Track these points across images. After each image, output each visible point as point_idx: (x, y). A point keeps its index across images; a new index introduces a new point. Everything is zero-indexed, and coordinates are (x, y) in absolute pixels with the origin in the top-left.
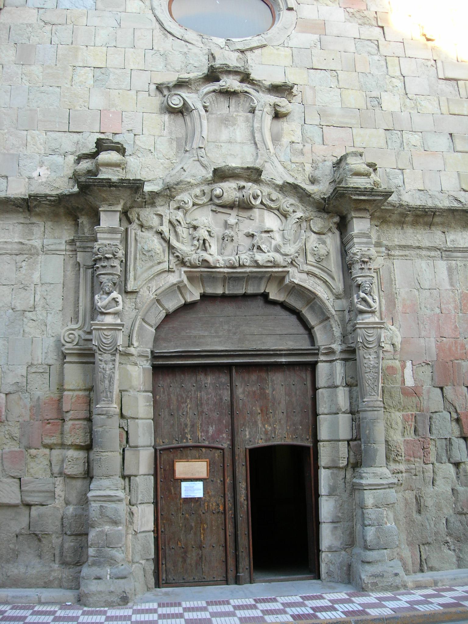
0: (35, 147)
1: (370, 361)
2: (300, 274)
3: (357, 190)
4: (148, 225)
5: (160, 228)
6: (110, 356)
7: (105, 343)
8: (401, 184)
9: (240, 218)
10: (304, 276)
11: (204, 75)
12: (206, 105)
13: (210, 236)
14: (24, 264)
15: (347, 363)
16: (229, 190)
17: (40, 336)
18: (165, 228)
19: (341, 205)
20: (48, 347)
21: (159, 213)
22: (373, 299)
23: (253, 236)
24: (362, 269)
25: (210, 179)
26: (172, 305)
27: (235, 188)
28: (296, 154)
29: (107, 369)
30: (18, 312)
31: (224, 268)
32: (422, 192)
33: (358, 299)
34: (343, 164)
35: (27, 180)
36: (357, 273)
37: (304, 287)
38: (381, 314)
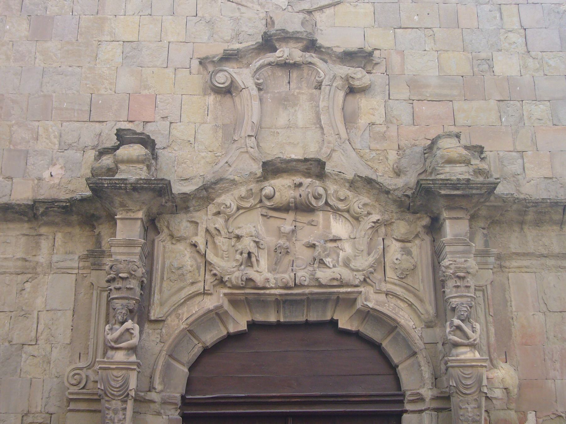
0: (47, 141)
1: (468, 412)
2: (377, 295)
3: (446, 183)
4: (179, 235)
5: (195, 239)
7: (113, 387)
8: (520, 171)
9: (298, 224)
10: (382, 297)
11: (257, 45)
12: (259, 82)
13: (259, 247)
15: (441, 414)
16: (282, 188)
19: (425, 202)
20: (51, 390)
21: (193, 219)
22: (473, 327)
23: (313, 246)
24: (457, 287)
25: (259, 174)
26: (211, 337)
27: (290, 186)
28: (376, 138)
30: (16, 346)
31: (276, 288)
32: (550, 181)
33: (451, 327)
34: (400, 147)
35: (36, 182)
36: (451, 292)
37: (381, 312)
38: (489, 347)
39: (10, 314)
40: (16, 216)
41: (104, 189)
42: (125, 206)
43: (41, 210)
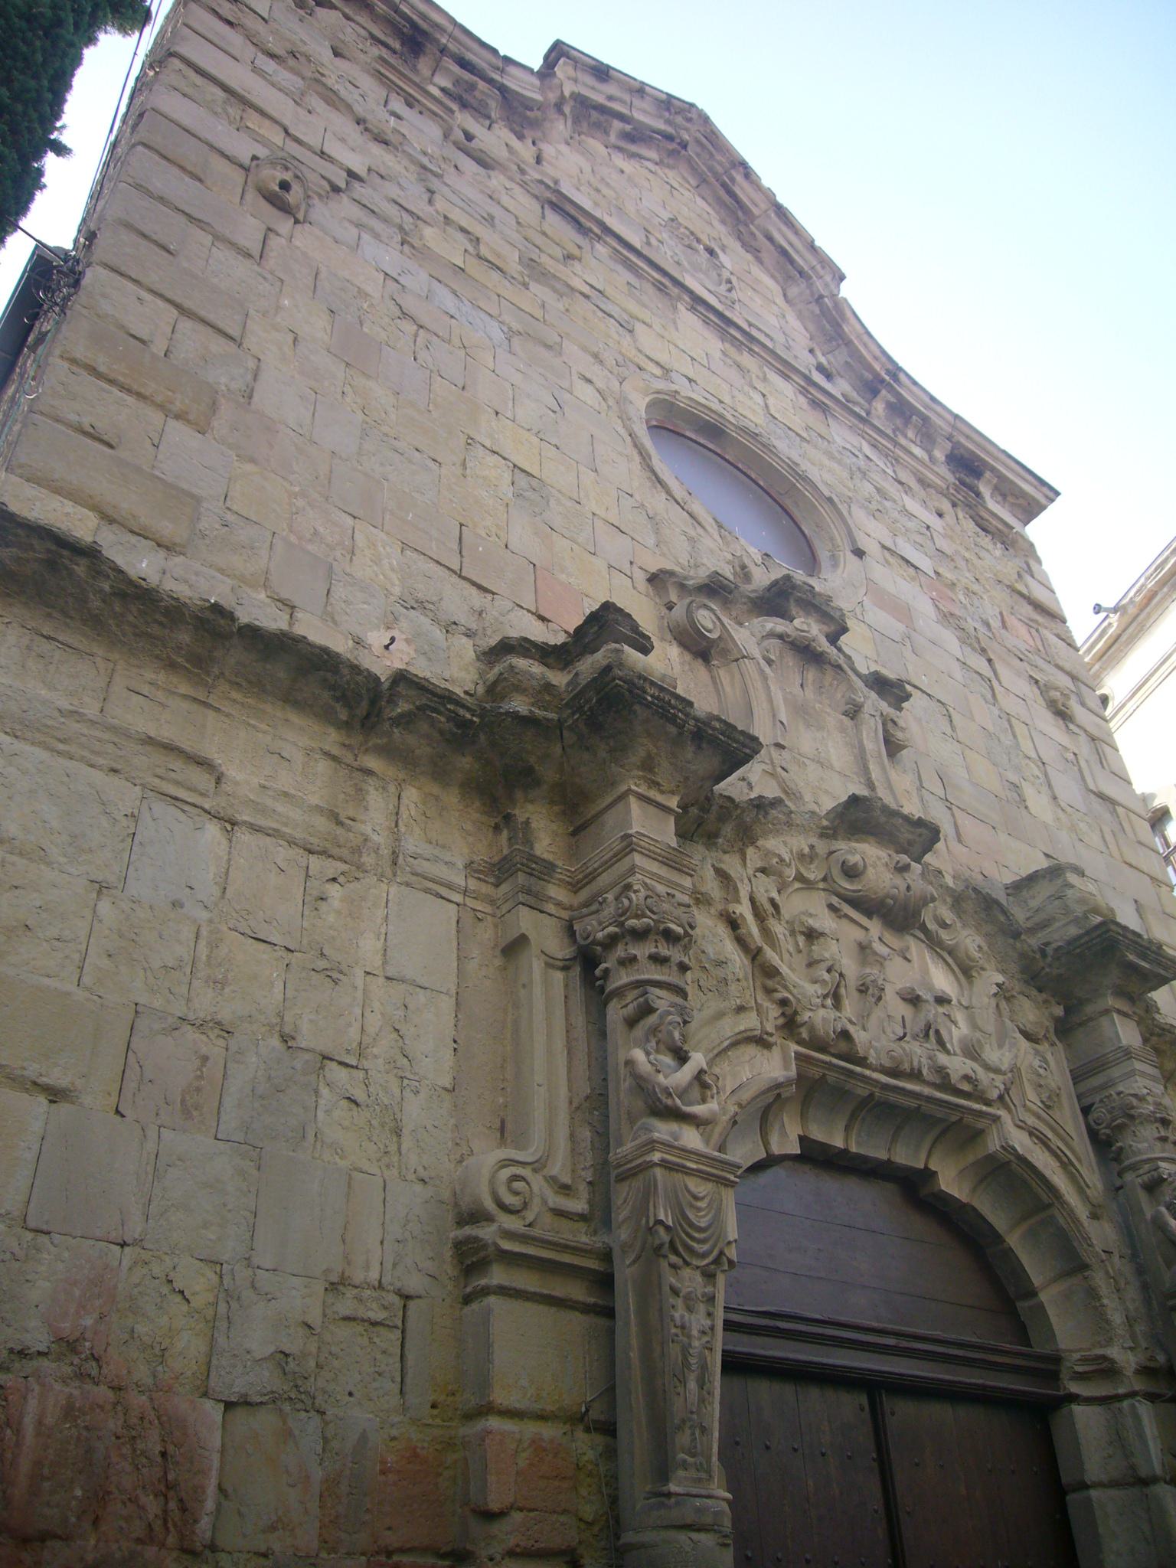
6: (699, 1279)
14: (334, 891)
17: (376, 1171)
18: (744, 909)
29: (695, 1333)
30: (307, 1056)
39: (284, 954)
40: (326, 695)
41: (637, 707)
42: (651, 770)
43: (403, 707)
